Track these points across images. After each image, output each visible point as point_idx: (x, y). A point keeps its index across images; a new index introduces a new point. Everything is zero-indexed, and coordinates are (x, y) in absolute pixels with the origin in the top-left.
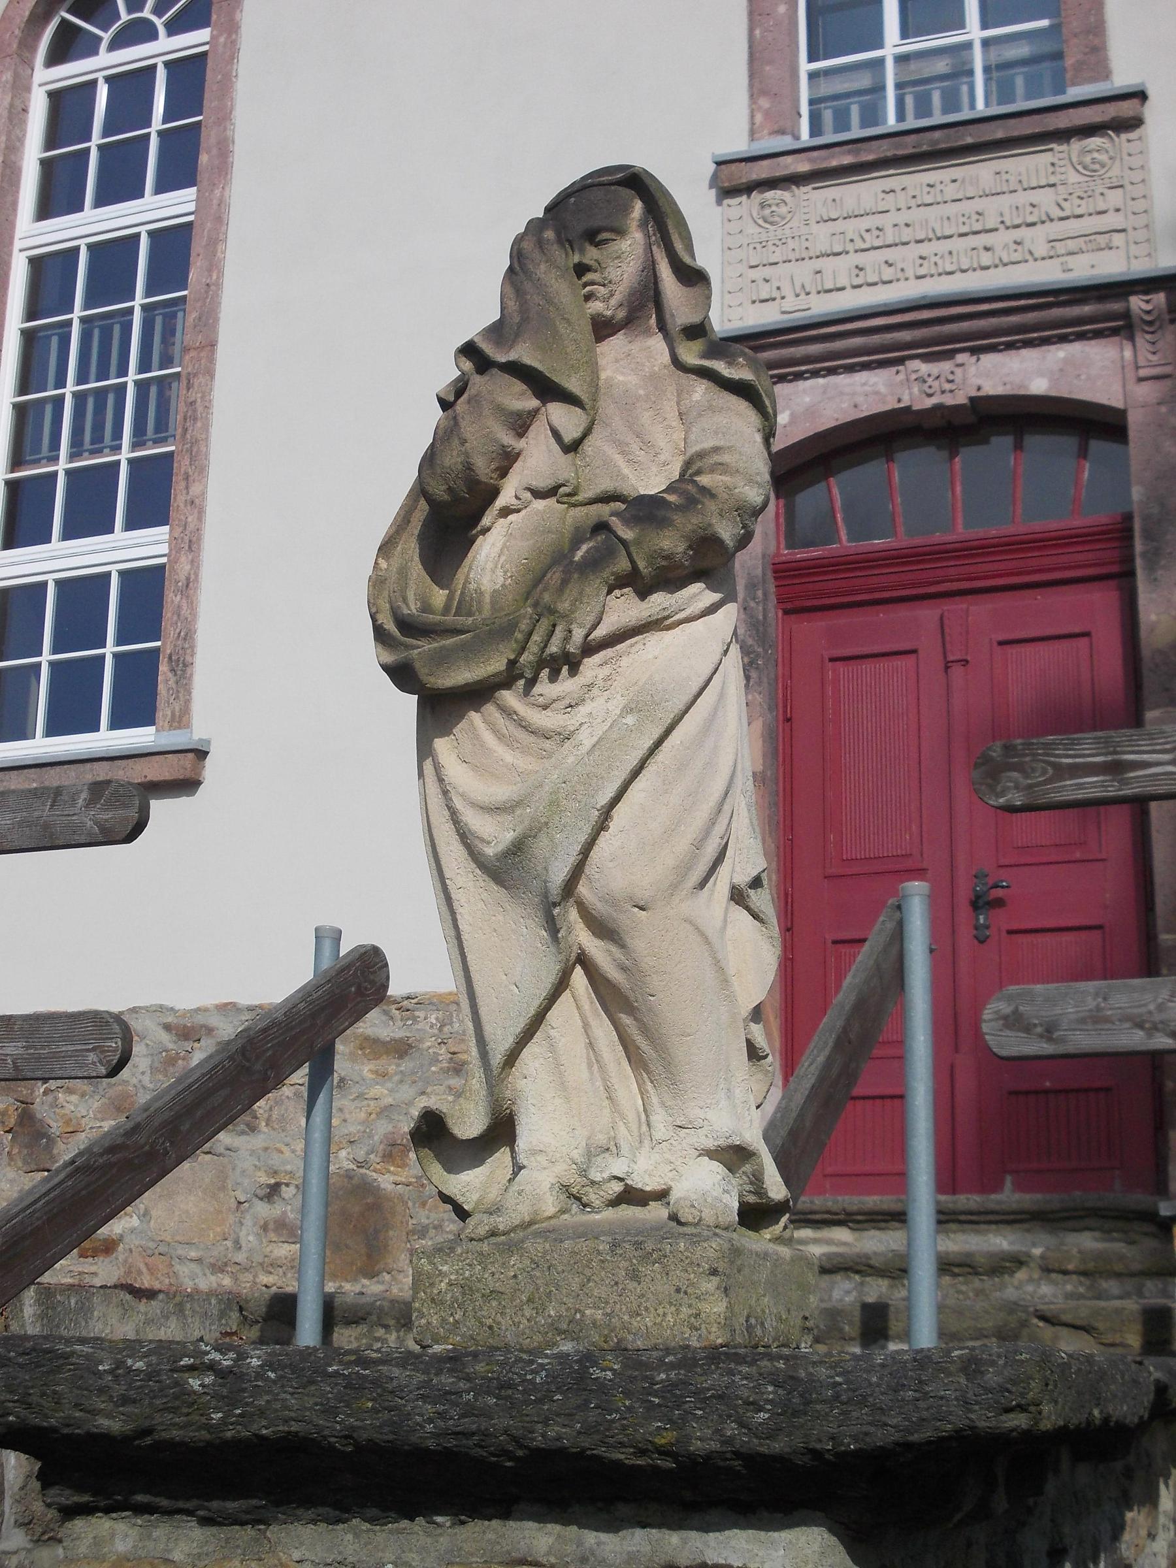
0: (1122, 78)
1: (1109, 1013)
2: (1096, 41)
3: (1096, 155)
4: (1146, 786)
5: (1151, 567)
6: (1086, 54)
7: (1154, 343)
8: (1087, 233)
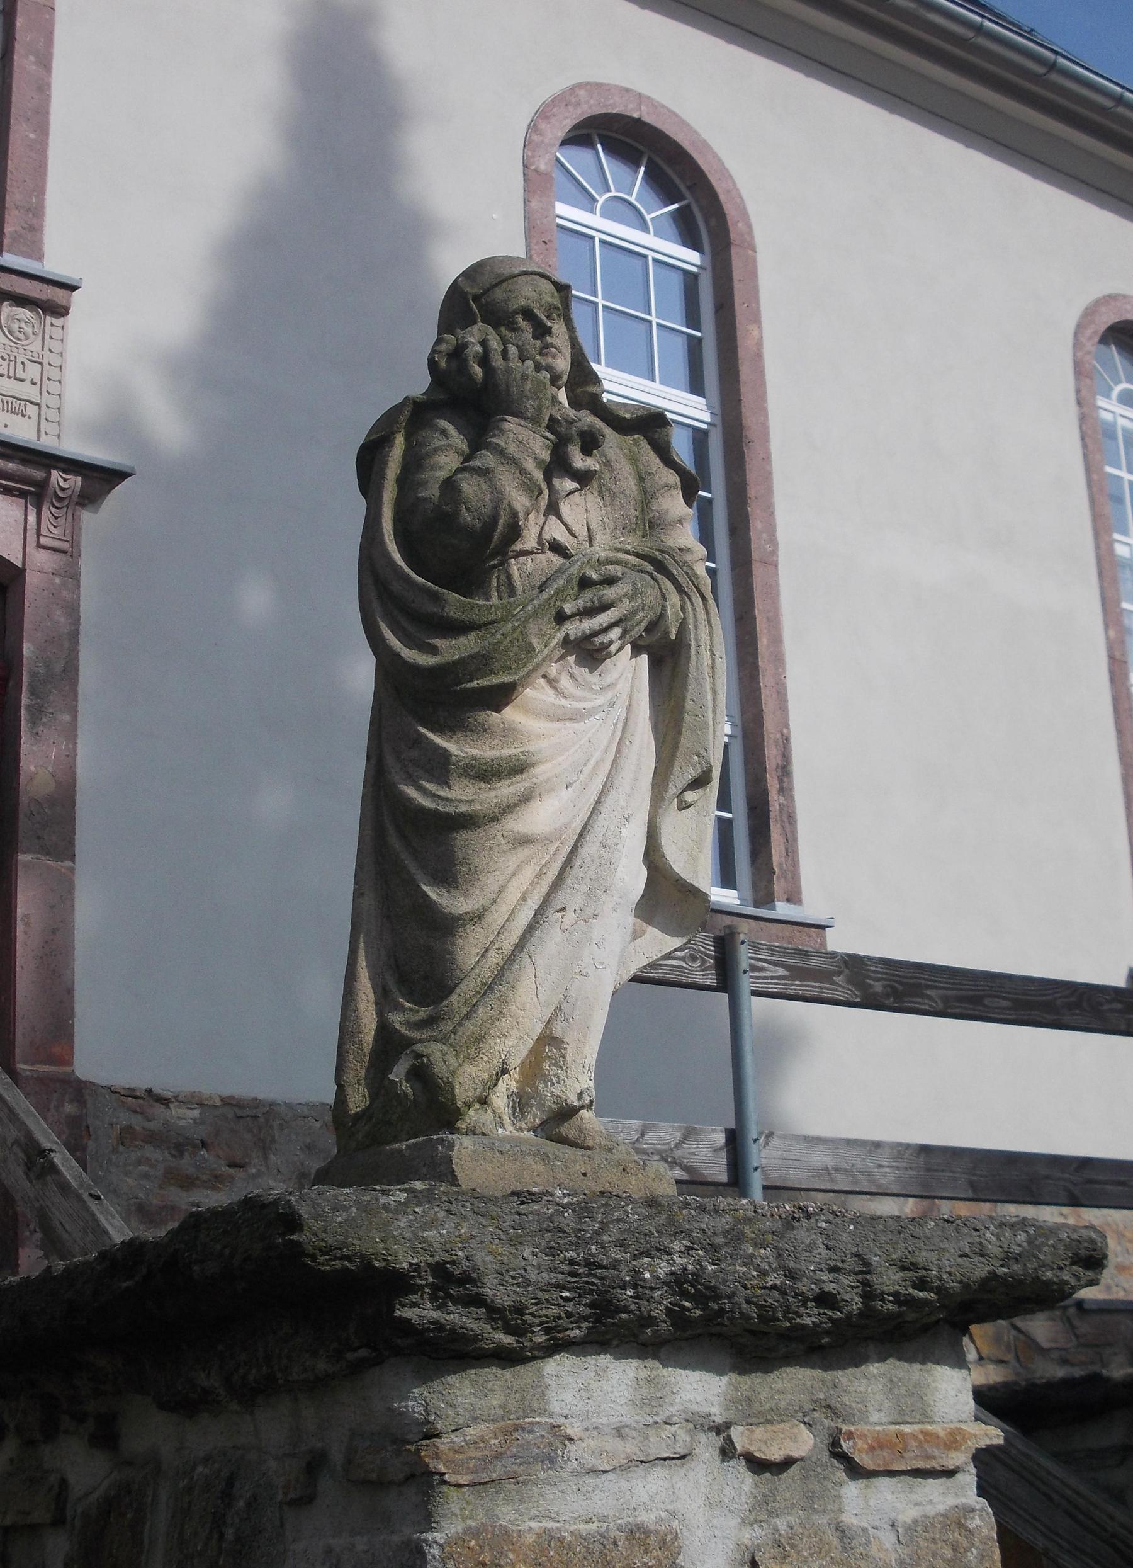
0: (54, 265)
1: (645, 1146)
2: (35, 221)
3: (23, 325)
4: (769, 988)
5: (34, 721)
6: (24, 229)
7: (56, 518)
8: (6, 393)
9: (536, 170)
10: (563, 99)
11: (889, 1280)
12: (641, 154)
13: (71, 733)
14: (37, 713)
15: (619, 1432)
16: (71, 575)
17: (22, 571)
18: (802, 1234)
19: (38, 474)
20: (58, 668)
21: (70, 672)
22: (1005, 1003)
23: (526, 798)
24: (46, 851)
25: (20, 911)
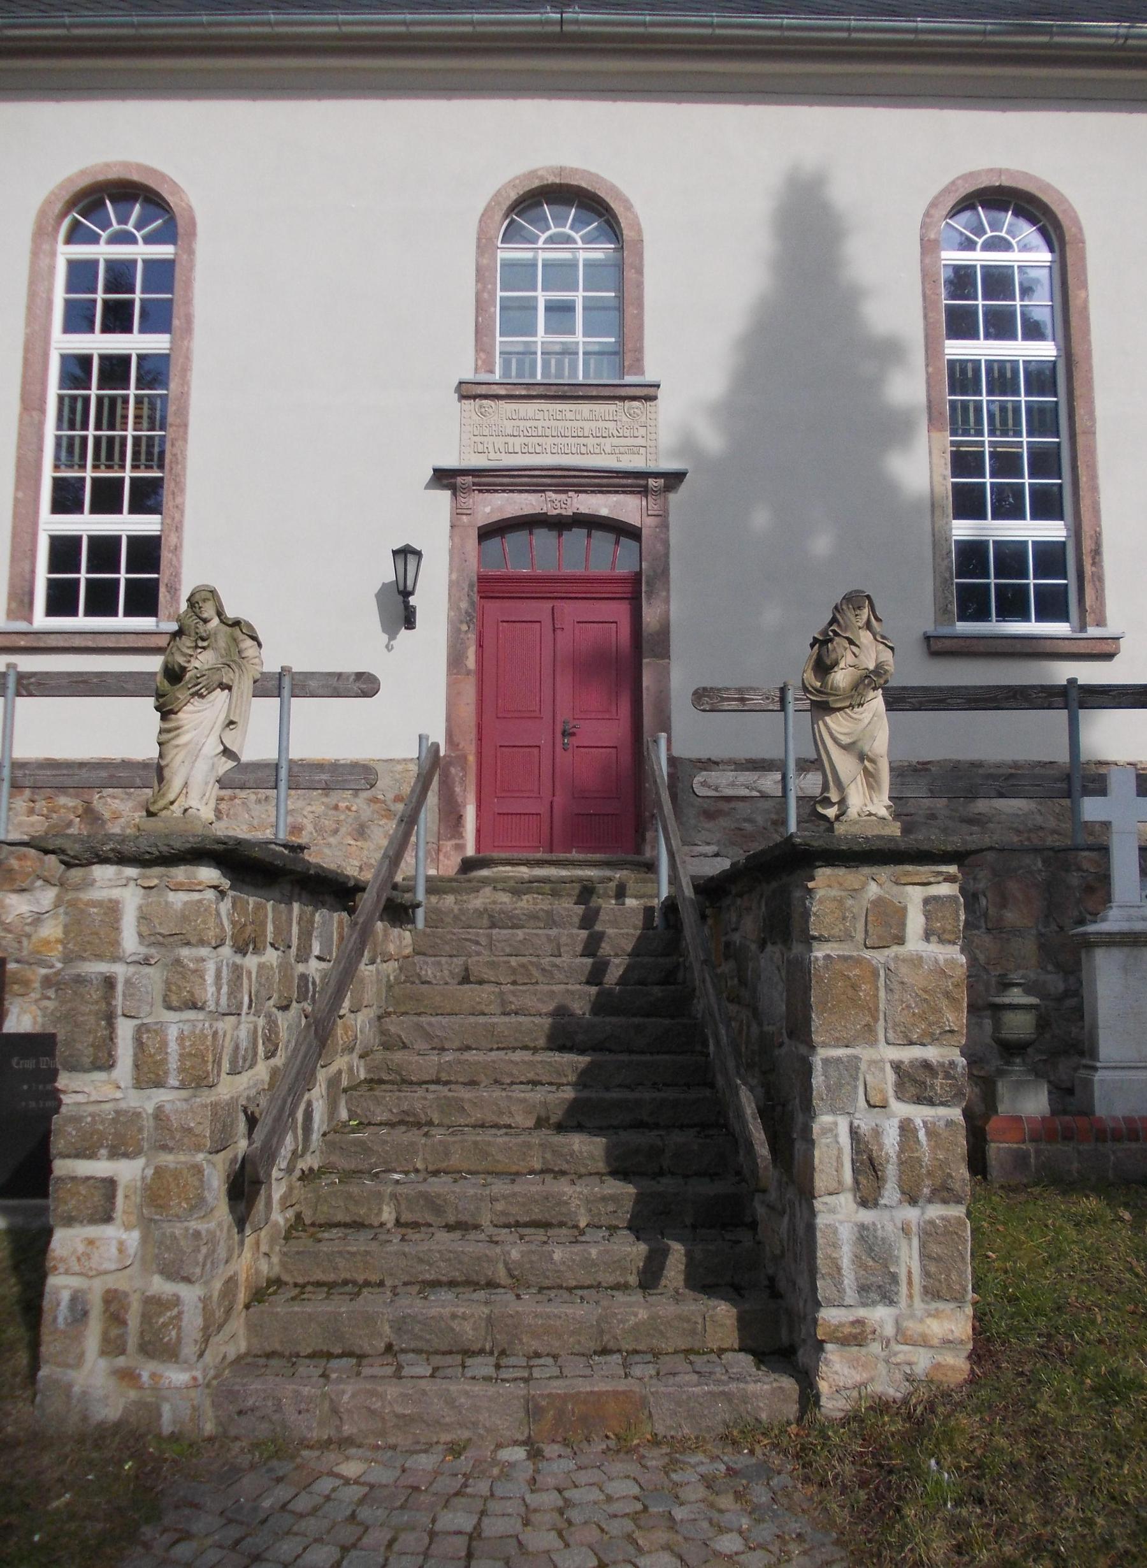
0: (649, 377)
5: (649, 598)
9: (929, 240)
10: (946, 191)
11: (164, 849)
12: (1010, 203)
13: (667, 601)
14: (650, 594)
15: (110, 880)
16: (664, 525)
17: (641, 529)
18: (141, 839)
19: (642, 482)
20: (659, 571)
21: (665, 572)
22: (959, 701)
23: (178, 735)
24: (655, 656)
25: (645, 684)
